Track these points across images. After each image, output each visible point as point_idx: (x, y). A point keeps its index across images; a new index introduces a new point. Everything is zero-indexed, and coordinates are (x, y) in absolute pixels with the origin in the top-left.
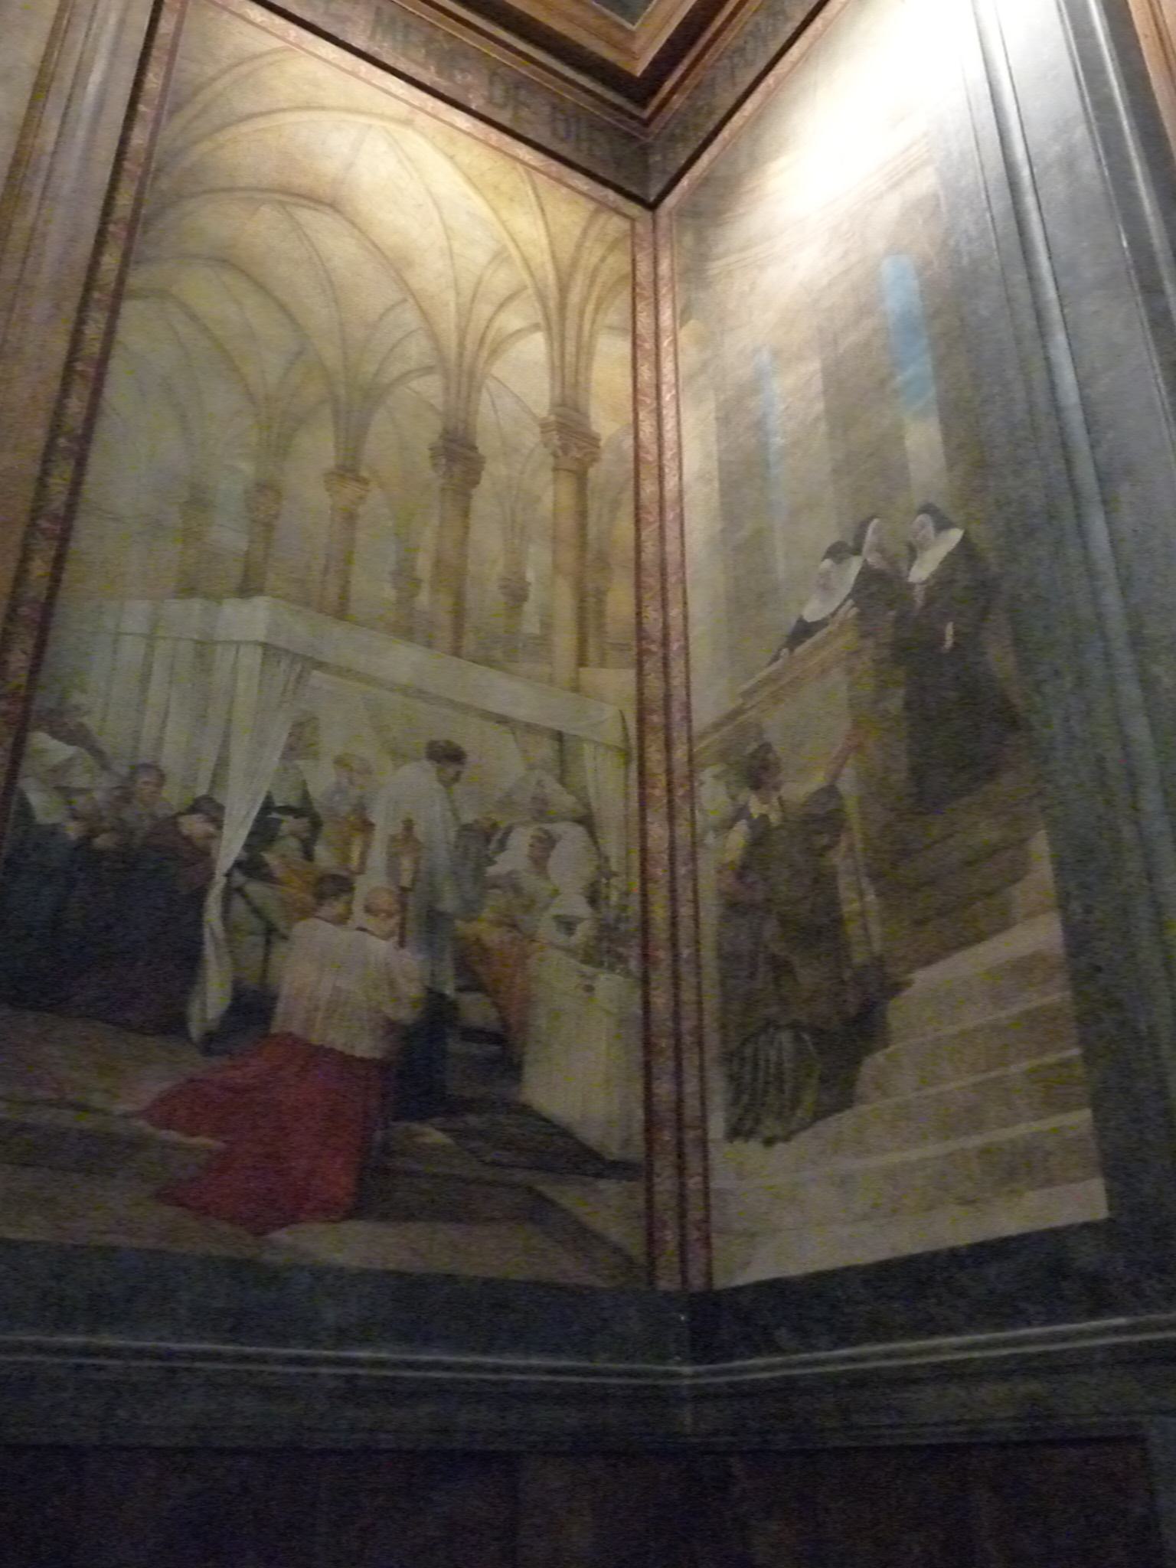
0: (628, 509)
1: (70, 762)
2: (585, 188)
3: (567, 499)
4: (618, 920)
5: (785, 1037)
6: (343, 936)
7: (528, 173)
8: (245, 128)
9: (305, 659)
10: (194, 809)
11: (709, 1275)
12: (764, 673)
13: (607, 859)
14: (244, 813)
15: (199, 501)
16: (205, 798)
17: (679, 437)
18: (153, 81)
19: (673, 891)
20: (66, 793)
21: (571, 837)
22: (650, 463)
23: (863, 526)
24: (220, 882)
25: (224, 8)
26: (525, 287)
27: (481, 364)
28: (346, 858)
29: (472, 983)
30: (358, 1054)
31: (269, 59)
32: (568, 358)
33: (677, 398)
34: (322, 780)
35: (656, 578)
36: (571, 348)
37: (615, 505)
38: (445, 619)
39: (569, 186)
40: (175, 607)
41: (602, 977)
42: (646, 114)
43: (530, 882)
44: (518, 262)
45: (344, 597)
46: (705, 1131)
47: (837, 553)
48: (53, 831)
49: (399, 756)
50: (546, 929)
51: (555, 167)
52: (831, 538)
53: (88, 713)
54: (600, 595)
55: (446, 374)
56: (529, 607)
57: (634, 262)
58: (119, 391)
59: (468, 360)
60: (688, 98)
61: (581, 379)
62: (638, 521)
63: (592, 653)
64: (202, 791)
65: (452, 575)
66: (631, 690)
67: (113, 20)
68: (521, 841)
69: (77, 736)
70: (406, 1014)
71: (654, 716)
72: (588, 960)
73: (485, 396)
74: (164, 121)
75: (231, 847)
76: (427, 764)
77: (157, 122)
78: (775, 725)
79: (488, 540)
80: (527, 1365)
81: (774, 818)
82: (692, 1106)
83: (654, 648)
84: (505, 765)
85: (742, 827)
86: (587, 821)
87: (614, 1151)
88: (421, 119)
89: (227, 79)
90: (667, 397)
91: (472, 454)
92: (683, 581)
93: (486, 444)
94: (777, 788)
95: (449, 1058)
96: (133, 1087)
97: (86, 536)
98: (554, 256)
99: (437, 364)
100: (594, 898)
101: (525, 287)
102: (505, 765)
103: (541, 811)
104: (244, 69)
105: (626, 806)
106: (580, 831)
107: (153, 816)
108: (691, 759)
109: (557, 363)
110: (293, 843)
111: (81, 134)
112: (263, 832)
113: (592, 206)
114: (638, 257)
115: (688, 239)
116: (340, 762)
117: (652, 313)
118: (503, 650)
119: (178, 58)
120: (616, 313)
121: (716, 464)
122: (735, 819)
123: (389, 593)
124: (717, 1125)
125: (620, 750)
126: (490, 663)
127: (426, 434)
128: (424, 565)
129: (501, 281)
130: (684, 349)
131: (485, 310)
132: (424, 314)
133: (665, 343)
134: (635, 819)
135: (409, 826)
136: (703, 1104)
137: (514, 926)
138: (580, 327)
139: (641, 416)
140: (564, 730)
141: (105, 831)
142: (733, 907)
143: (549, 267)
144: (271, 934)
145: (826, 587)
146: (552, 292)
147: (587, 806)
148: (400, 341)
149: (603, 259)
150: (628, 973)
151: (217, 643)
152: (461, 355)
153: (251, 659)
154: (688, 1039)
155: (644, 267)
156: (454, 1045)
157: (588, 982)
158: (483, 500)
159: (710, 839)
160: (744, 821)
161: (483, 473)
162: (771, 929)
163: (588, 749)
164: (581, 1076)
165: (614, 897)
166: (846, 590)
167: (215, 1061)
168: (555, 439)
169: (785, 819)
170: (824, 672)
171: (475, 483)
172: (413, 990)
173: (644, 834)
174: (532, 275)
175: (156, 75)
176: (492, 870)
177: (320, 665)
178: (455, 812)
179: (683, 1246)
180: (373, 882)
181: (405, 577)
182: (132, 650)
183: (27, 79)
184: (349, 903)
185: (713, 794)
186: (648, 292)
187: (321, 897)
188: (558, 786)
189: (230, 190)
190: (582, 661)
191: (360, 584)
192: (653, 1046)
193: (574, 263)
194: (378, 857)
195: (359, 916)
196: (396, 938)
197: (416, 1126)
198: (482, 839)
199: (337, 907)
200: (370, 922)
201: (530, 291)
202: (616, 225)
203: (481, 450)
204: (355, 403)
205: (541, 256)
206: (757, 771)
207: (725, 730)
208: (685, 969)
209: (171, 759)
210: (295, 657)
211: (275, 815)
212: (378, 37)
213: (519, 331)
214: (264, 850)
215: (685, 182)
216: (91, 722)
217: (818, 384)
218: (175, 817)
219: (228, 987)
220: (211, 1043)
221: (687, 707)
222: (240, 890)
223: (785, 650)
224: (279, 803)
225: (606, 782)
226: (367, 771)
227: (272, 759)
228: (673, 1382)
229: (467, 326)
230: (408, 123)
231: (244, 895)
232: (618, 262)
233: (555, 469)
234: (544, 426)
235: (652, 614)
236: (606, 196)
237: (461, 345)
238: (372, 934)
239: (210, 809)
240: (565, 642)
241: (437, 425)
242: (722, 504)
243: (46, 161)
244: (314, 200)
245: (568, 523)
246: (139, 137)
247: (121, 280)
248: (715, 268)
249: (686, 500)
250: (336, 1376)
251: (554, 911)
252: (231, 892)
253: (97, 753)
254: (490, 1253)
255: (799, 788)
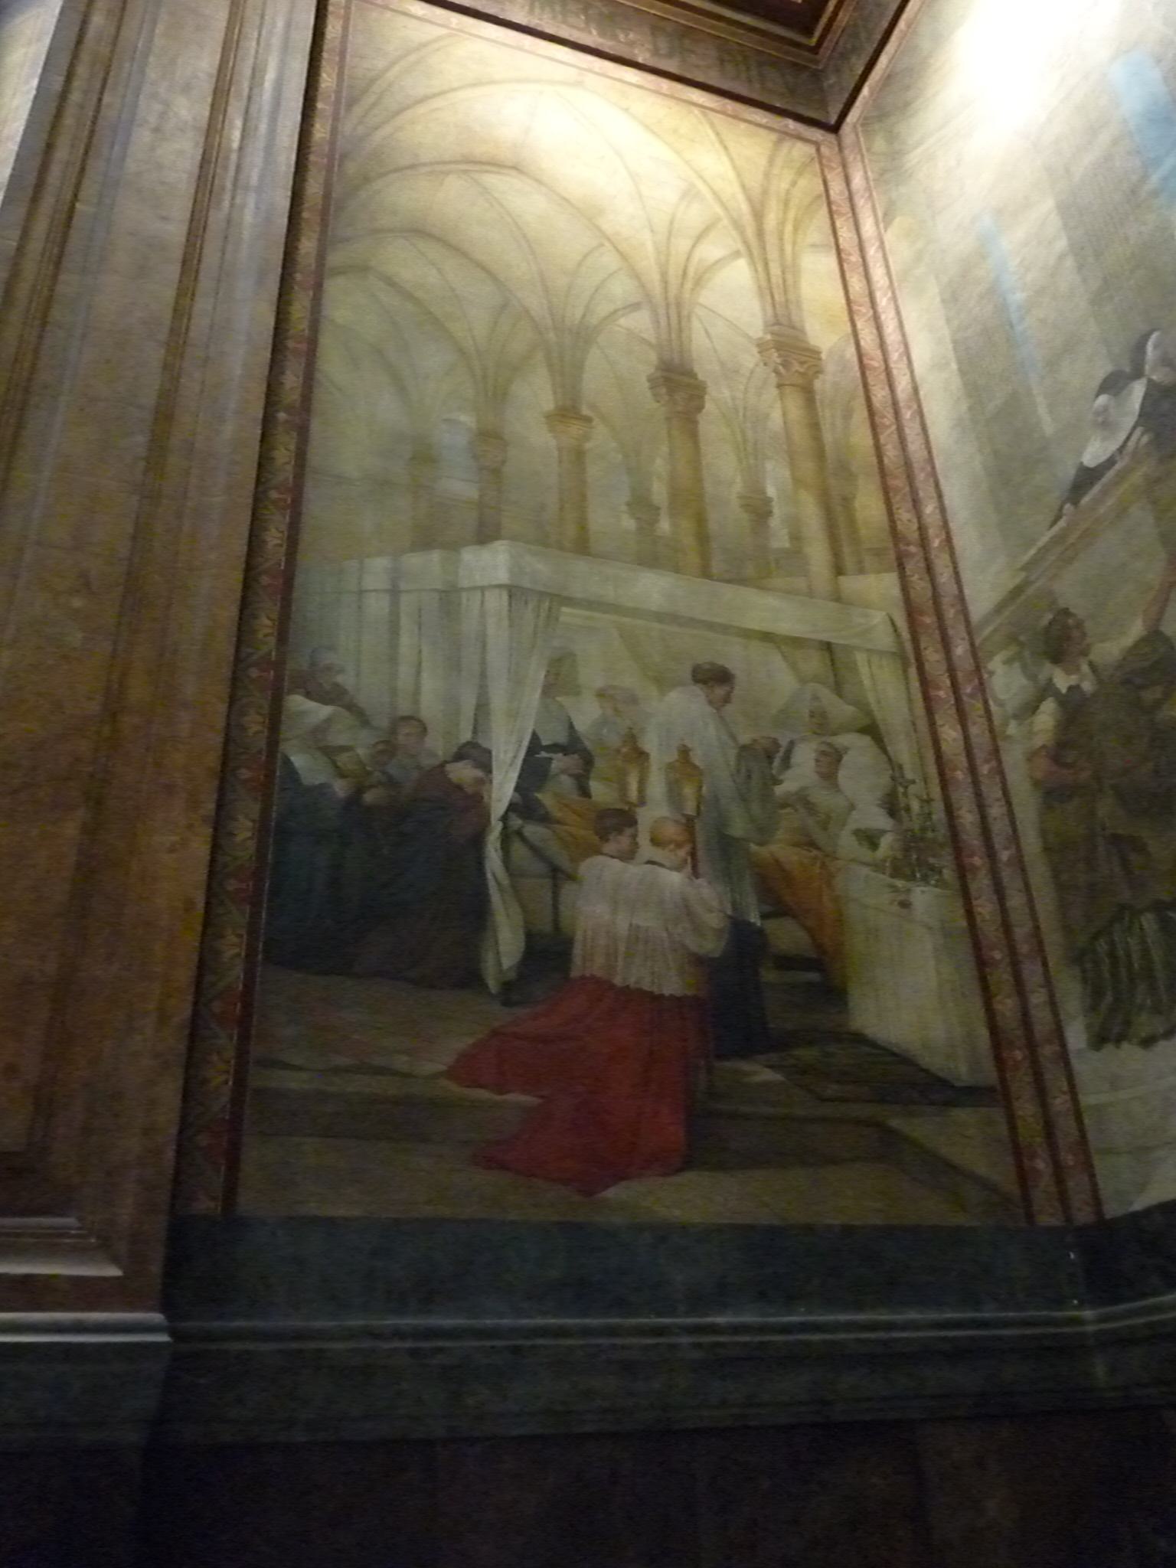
0: (860, 414)
1: (329, 721)
2: (764, 121)
3: (795, 408)
4: (923, 829)
5: (1149, 922)
6: (634, 871)
7: (705, 115)
8: (421, 110)
9: (553, 596)
10: (459, 756)
11: (1097, 1201)
12: (1043, 540)
13: (901, 767)
14: (510, 755)
15: (424, 457)
16: (468, 743)
17: (904, 335)
18: (327, 80)
19: (978, 795)
20: (330, 753)
21: (858, 750)
22: (875, 368)
23: (1140, 348)
24: (496, 827)
25: (386, 7)
26: (719, 219)
27: (687, 295)
28: (623, 789)
29: (778, 909)
30: (667, 992)
31: (436, 46)
32: (774, 280)
33: (894, 298)
34: (586, 715)
35: (903, 478)
36: (775, 270)
37: (848, 415)
38: (689, 541)
39: (749, 122)
40: (414, 561)
41: (918, 890)
42: (813, 41)
43: (822, 797)
44: (709, 196)
45: (583, 527)
46: (1063, 1045)
47: (1113, 384)
48: (322, 789)
49: (663, 683)
50: (847, 843)
51: (730, 105)
52: (1103, 369)
53: (342, 671)
54: (847, 501)
55: (654, 312)
56: (775, 522)
57: (825, 183)
58: (332, 364)
59: (673, 291)
60: (855, 9)
61: (792, 297)
62: (874, 427)
63: (849, 562)
64: (466, 736)
65: (690, 498)
66: (896, 592)
67: (280, 24)
68: (805, 757)
69: (334, 696)
70: (712, 946)
71: (928, 615)
72: (896, 873)
73: (696, 324)
74: (342, 112)
75: (503, 789)
76: (697, 690)
77: (336, 118)
78: (1070, 589)
79: (724, 467)
80: (912, 1320)
81: (1088, 686)
82: (1041, 1017)
83: (913, 549)
84: (777, 681)
85: (1049, 706)
86: (872, 730)
87: (962, 1072)
88: (590, 80)
89: (396, 69)
90: (883, 301)
91: (692, 381)
92: (933, 473)
93: (705, 369)
94: (1085, 653)
95: (770, 984)
96: (433, 1047)
97: (318, 506)
98: (743, 187)
99: (643, 300)
100: (892, 806)
101: (719, 219)
102: (777, 681)
103: (821, 723)
104: (412, 58)
105: (911, 709)
106: (866, 740)
107: (419, 767)
108: (974, 651)
109: (764, 284)
110: (567, 783)
111: (263, 127)
112: (534, 772)
113: (774, 137)
114: (829, 177)
115: (880, 144)
116: (601, 694)
117: (853, 228)
118: (756, 565)
119: (348, 57)
120: (817, 228)
121: (950, 347)
122: (1040, 699)
123: (629, 523)
124: (1076, 1036)
125: (893, 653)
126: (742, 581)
127: (642, 368)
128: (659, 492)
129: (694, 216)
130: (893, 247)
131: (682, 245)
132: (623, 256)
133: (872, 251)
134: (923, 725)
135: (685, 752)
136: (1055, 1014)
137: (812, 844)
138: (782, 250)
139: (859, 325)
140: (833, 641)
141: (371, 786)
142: (1052, 795)
143: (741, 197)
144: (558, 876)
145: (1105, 425)
146: (748, 219)
147: (869, 713)
148: (604, 281)
149: (794, 184)
150: (942, 884)
151: (463, 589)
152: (666, 289)
153: (497, 602)
154: (1024, 948)
155: (837, 187)
156: (769, 975)
157: (902, 897)
158: (711, 423)
159: (1012, 729)
160: (1050, 699)
161: (707, 397)
162: (1106, 808)
163: (860, 658)
164: (912, 995)
165: (915, 806)
166: (1130, 421)
167: (521, 1012)
168: (775, 356)
169: (1100, 681)
170: (1122, 511)
171: (700, 408)
172: (714, 921)
173: (936, 742)
174: (726, 209)
175: (329, 76)
176: (779, 790)
177: (569, 601)
178: (733, 737)
179: (1059, 1172)
180: (656, 811)
181: (641, 504)
182: (377, 606)
183: (206, 87)
184: (634, 836)
185: (1007, 682)
186: (845, 208)
187: (604, 836)
188: (835, 698)
189: (412, 167)
190: (839, 570)
191: (599, 518)
192: (987, 960)
193: (765, 192)
194: (657, 787)
195: (646, 850)
196: (689, 868)
197: (745, 1066)
198: (764, 759)
199: (624, 841)
200: (658, 854)
201: (725, 222)
202: (800, 151)
203: (700, 377)
204: (566, 346)
205: (731, 189)
206: (1059, 640)
207: (1007, 613)
208: (1007, 875)
209: (430, 707)
210: (542, 594)
211: (544, 754)
212: (537, 11)
213: (717, 262)
214: (539, 789)
215: (865, 91)
216: (346, 680)
217: (1055, 222)
218: (442, 765)
219: (522, 937)
220: (511, 991)
221: (961, 598)
222: (519, 833)
223: (1068, 506)
224: (545, 742)
225: (887, 690)
226: (634, 700)
227: (533, 697)
228: (1079, 1329)
229: (667, 261)
230: (579, 84)
231: (524, 840)
232: (810, 184)
233: (779, 386)
234: (762, 347)
235: (904, 515)
236: (786, 126)
237: (665, 282)
238: (661, 865)
239: (477, 754)
240: (818, 553)
241: (653, 357)
242: (965, 384)
243: (234, 157)
244: (495, 165)
245: (801, 436)
246: (320, 131)
247: (321, 257)
248: (913, 158)
249: (922, 393)
250: (698, 1346)
251: (852, 825)
252: (506, 838)
253: (352, 708)
254: (849, 1198)
255: (1114, 643)
